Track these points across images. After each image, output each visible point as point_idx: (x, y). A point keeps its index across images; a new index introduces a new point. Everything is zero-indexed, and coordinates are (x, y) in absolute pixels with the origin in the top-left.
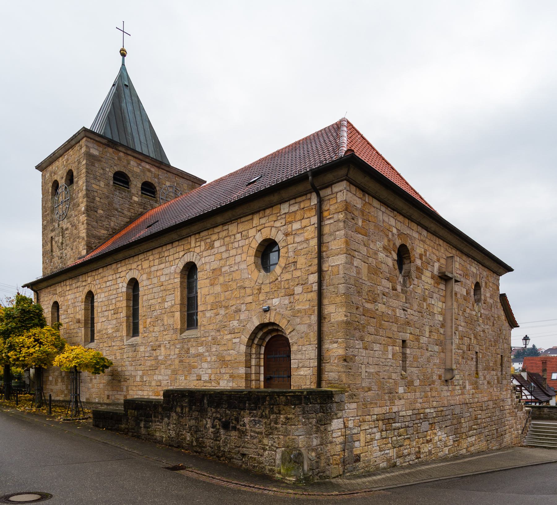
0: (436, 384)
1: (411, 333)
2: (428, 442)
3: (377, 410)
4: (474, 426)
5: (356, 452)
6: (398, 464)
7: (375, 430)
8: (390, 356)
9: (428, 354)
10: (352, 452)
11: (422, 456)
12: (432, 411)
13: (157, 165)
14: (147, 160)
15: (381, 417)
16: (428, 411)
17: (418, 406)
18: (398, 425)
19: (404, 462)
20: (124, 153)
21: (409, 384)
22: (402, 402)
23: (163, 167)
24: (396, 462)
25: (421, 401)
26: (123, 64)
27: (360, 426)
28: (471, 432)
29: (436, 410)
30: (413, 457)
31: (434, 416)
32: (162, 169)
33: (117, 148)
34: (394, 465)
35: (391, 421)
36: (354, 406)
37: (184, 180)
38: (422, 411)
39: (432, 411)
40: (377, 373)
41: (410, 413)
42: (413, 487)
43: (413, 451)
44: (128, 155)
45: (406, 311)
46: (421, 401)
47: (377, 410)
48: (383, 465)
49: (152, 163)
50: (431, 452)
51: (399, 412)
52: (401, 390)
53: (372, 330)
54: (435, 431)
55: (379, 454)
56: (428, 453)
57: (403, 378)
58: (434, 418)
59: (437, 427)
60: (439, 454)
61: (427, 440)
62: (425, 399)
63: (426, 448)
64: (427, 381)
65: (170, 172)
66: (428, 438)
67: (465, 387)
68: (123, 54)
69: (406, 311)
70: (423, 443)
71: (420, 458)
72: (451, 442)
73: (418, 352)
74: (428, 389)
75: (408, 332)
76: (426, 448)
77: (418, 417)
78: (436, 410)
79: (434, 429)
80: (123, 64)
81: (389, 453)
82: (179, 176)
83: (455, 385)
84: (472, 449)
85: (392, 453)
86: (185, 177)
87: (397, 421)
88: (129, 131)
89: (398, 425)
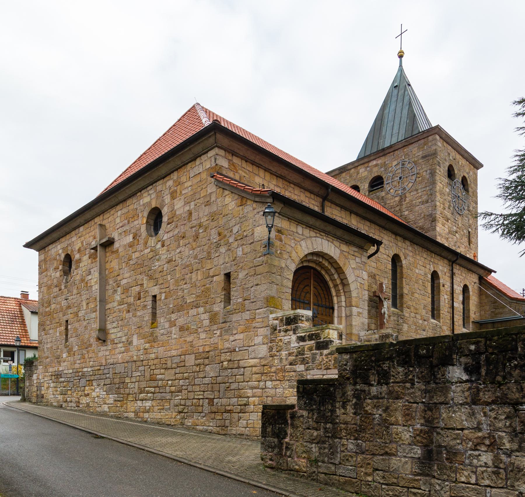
0: (93, 346)
1: (71, 313)
2: (87, 395)
3: (51, 370)
4: (147, 389)
5: (43, 393)
6: (63, 406)
7: (51, 381)
8: (58, 334)
9: (85, 323)
10: (41, 392)
11: (81, 406)
12: (89, 369)
13: (382, 154)
14: (372, 158)
15: (53, 373)
16: (85, 370)
17: (77, 366)
18: (63, 379)
19: (68, 407)
20: (354, 168)
21: (70, 352)
22: (65, 364)
23: (387, 151)
24: (62, 405)
25: (78, 362)
26: (401, 65)
27: (43, 378)
28: (142, 395)
29: (92, 369)
30: (74, 405)
31: (91, 374)
32: (389, 153)
33: (347, 169)
34: (61, 406)
35: (59, 377)
36: (41, 367)
37: (413, 145)
38: (80, 370)
39: (89, 369)
40: (51, 347)
41: (71, 371)
42: (192, 467)
43: (74, 399)
44: (357, 166)
45: (68, 299)
46: (78, 362)
47: (51, 370)
48: (55, 404)
49: (378, 156)
50: (89, 405)
51: (63, 370)
52: (64, 355)
53: (48, 322)
54: (93, 388)
55: (52, 396)
56: (86, 405)
57: (66, 347)
58: (91, 375)
59: (95, 384)
60: (97, 409)
61: (85, 394)
62: (82, 360)
63: (84, 400)
64: (86, 346)
65: (397, 150)
66: (86, 392)
67: (130, 343)
68: (401, 57)
69: (68, 299)
70: (82, 396)
71: (79, 407)
72: (111, 401)
73: (77, 325)
74: (85, 352)
75: (69, 313)
76: (84, 400)
77: (77, 375)
78: (92, 369)
79: (92, 385)
80: (401, 65)
81: (58, 397)
82: (406, 146)
83: (116, 343)
84: (146, 415)
85: (60, 397)
86: (413, 141)
87: (62, 377)
88: (383, 133)
89: (63, 379)
